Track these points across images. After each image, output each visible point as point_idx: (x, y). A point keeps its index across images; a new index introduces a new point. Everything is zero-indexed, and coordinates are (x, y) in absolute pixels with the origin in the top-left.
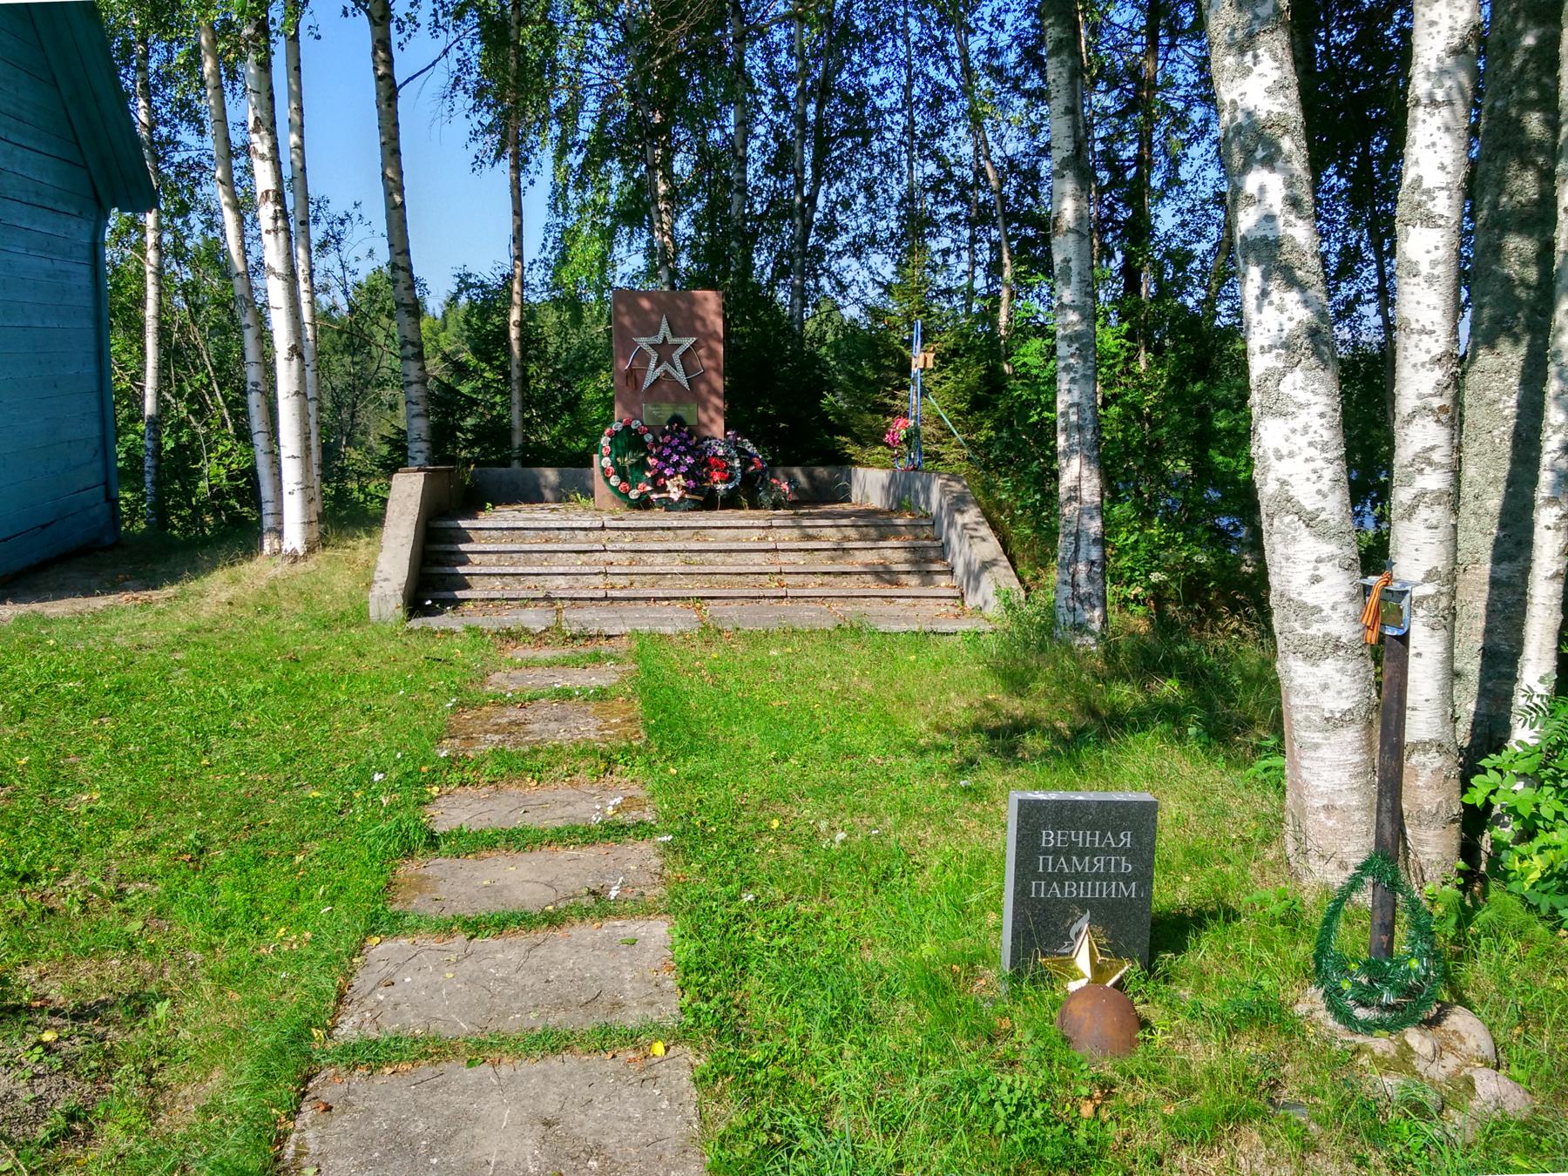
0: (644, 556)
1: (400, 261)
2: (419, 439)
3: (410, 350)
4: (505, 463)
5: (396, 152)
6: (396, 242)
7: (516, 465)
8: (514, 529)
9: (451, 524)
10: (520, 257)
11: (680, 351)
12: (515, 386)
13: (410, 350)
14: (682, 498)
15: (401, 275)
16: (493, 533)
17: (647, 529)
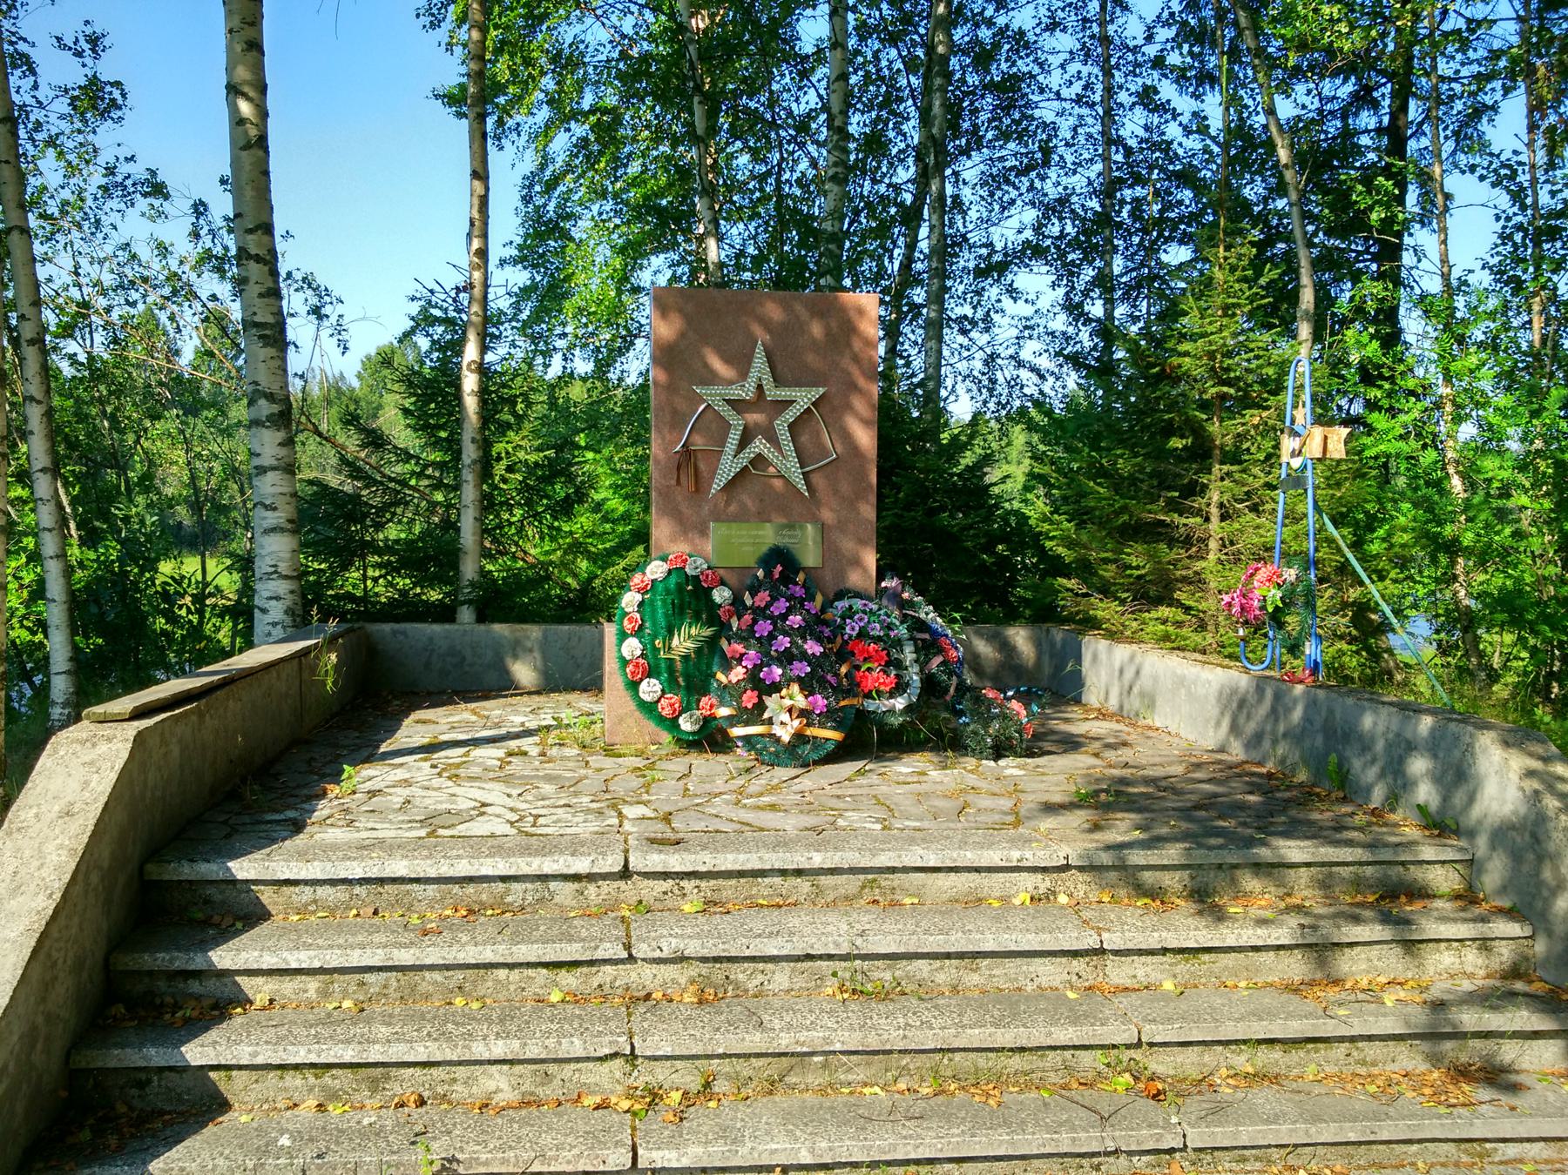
0: (739, 973)
1: (254, 244)
2: (275, 573)
3: (265, 408)
4: (445, 613)
5: (255, 47)
6: (247, 210)
7: (466, 614)
8: (381, 881)
9: (208, 869)
10: (483, 253)
11: (791, 415)
12: (469, 476)
13: (265, 408)
14: (799, 737)
15: (254, 269)
16: (324, 892)
17: (741, 874)
